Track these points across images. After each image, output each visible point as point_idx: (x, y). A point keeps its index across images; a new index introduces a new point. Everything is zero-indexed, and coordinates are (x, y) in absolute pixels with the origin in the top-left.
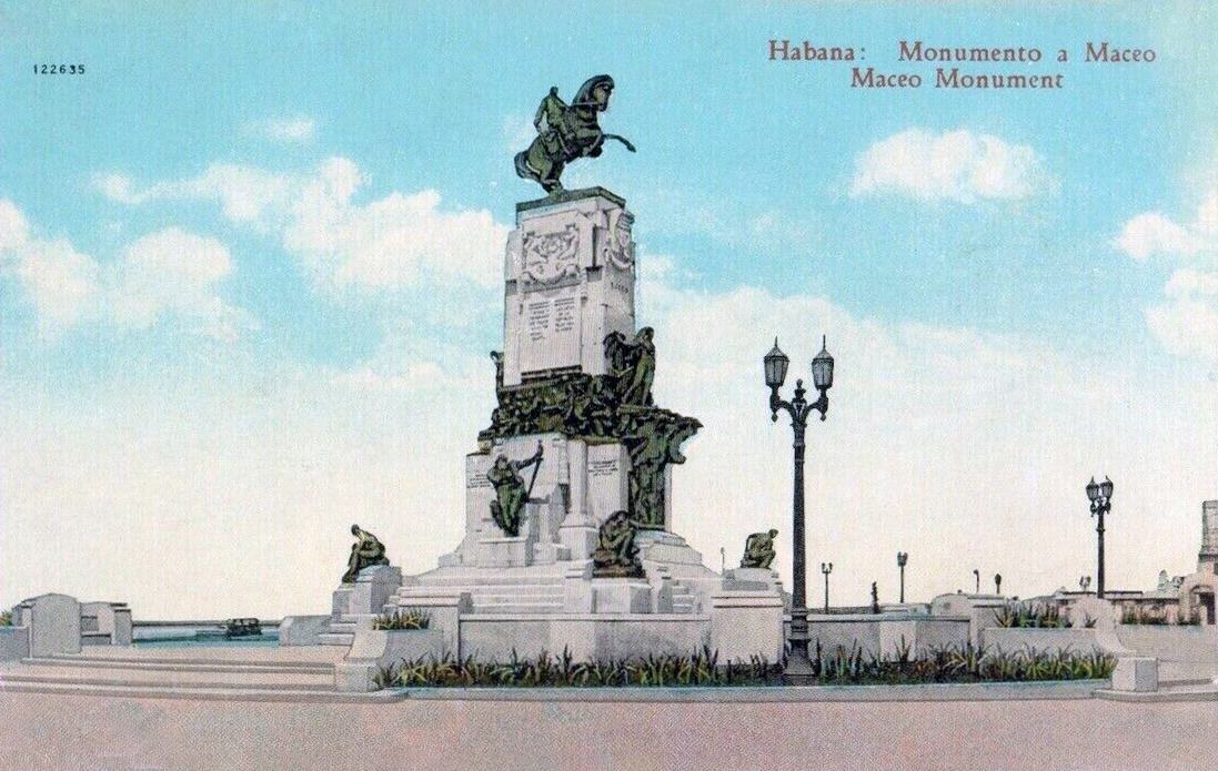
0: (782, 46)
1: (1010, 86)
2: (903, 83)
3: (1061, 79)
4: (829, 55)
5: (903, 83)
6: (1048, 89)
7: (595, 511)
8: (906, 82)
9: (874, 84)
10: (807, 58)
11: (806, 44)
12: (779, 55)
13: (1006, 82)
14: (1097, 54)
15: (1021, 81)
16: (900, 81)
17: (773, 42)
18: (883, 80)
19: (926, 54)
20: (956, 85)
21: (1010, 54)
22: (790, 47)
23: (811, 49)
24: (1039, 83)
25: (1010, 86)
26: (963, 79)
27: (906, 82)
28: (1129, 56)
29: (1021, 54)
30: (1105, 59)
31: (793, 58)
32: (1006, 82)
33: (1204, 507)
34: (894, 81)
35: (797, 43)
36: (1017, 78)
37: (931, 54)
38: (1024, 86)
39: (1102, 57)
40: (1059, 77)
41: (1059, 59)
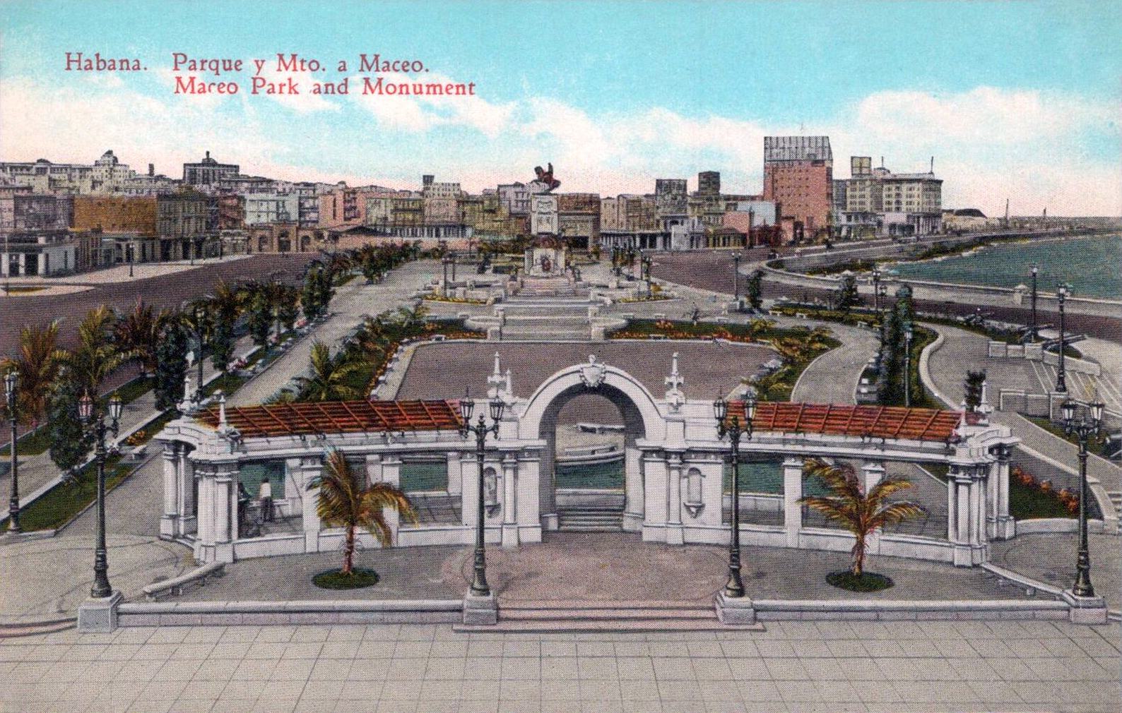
0: (76, 58)
1: (428, 93)
2: (111, 63)
3: (473, 88)
4: (118, 65)
5: (450, 91)
6: (404, 97)
7: (73, 252)
8: (409, 68)
9: (380, 69)
10: (98, 68)
11: (97, 55)
12: (74, 66)
13: (425, 89)
14: (370, 65)
15: (438, 89)
16: (403, 67)
17: (69, 54)
18: (388, 66)
19: (338, 89)
20: (381, 93)
21: (330, 88)
22: (83, 58)
23: (102, 60)
24: (454, 90)
25: (428, 93)
26: (339, 87)
27: (409, 68)
28: (398, 66)
29: (281, 88)
30: (193, 92)
31: (199, 92)
32: (425, 89)
33: (235, 166)
34: (398, 66)
35: (89, 54)
36: (434, 86)
37: (391, 89)
38: (441, 93)
39: (374, 68)
40: (471, 85)
41: (340, 70)
